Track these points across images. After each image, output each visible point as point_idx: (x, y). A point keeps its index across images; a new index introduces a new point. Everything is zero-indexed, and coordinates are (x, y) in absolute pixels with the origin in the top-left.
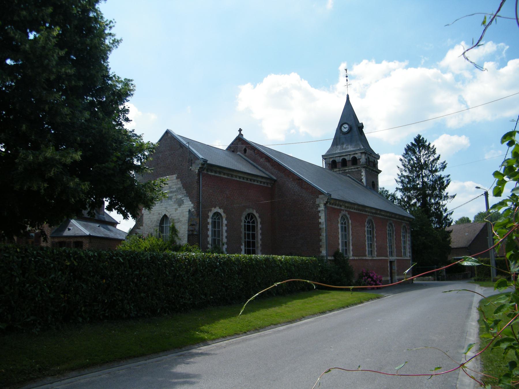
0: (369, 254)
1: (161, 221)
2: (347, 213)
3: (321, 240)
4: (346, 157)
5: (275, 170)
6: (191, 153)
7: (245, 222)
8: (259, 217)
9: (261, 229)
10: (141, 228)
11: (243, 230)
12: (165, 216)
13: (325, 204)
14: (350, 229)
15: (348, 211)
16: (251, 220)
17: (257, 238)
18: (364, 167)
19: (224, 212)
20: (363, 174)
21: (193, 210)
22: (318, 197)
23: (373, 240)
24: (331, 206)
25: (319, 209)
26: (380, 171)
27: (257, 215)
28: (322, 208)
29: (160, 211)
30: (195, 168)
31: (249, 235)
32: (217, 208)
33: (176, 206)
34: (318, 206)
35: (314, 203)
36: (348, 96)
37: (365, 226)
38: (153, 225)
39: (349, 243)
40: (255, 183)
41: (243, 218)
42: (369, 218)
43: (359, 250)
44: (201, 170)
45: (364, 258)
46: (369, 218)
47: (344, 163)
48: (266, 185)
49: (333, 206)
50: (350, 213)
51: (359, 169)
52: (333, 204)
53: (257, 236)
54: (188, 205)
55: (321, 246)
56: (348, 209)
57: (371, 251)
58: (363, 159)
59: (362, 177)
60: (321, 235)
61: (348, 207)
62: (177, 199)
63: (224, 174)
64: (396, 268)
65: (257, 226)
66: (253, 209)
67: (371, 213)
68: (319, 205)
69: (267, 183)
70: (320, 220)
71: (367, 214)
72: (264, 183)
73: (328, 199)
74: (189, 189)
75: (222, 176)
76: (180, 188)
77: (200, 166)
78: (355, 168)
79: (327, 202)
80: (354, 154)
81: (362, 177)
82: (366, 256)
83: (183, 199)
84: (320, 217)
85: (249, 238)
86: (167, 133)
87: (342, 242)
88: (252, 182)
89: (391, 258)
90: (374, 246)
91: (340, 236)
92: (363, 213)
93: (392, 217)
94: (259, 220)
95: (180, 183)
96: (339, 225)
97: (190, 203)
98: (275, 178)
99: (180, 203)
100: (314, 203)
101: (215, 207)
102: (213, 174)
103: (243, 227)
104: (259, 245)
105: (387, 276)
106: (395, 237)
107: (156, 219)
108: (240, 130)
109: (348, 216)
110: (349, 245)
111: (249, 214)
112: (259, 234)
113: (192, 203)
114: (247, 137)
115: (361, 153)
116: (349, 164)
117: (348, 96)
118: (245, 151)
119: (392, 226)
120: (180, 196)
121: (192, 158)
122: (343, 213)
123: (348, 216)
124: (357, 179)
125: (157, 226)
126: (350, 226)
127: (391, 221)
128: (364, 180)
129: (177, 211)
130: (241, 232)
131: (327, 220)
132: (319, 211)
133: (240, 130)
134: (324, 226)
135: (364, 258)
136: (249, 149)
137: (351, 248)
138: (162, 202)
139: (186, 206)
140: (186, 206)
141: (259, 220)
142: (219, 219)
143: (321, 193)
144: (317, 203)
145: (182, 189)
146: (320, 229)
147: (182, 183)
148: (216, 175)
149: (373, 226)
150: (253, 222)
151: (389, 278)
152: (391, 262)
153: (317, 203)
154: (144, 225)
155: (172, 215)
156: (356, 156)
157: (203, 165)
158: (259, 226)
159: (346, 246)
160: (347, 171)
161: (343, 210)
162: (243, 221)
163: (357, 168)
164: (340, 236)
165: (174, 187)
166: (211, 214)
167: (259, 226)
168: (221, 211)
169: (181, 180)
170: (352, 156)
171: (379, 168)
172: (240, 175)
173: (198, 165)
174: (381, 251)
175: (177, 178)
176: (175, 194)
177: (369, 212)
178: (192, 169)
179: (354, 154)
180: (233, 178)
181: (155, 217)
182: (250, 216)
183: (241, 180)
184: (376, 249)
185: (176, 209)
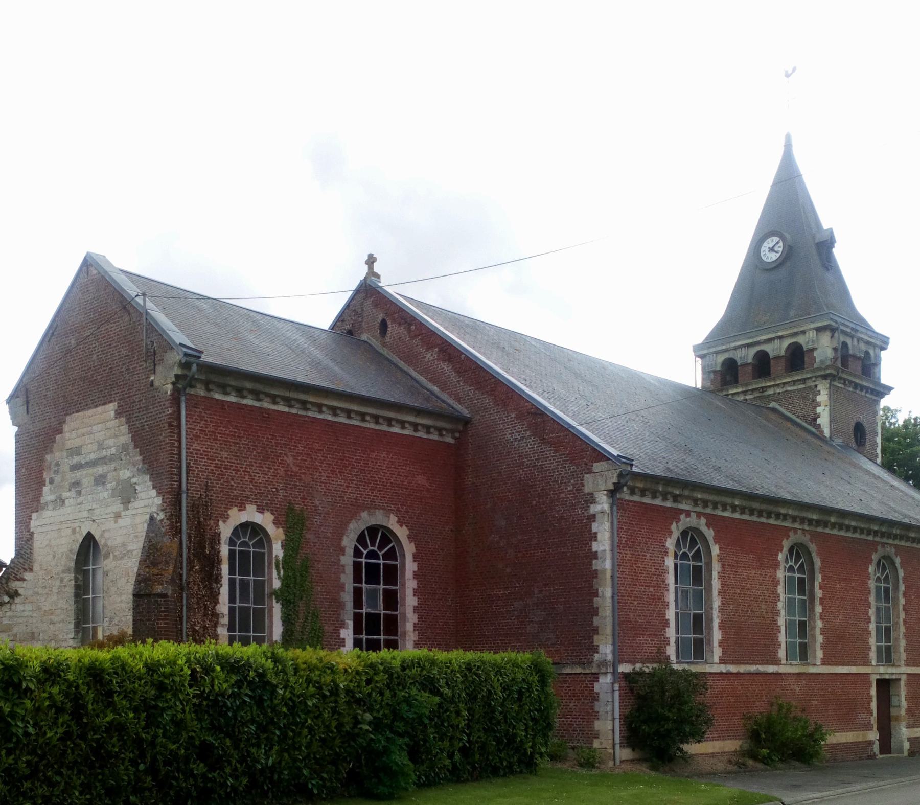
0: (879, 659)
1: (79, 554)
2: (703, 521)
3: (595, 612)
4: (767, 348)
5: (467, 388)
6: (153, 328)
7: (357, 553)
8: (409, 537)
9: (416, 575)
10: (27, 576)
11: (347, 579)
12: (89, 538)
13: (612, 493)
14: (715, 574)
15: (707, 516)
16: (381, 548)
17: (404, 605)
18: (825, 377)
19: (276, 523)
20: (823, 397)
21: (161, 516)
22: (590, 472)
23: (812, 609)
24: (636, 498)
25: (594, 509)
26: (889, 389)
27: (402, 533)
28: (603, 504)
29: (76, 525)
30: (164, 380)
31: (244, 585)
32: (251, 508)
33: (117, 507)
34: (591, 499)
35: (579, 490)
36: (788, 139)
37: (776, 565)
38: (60, 569)
39: (710, 620)
40: (396, 430)
41: (349, 542)
42: (793, 538)
43: (751, 639)
44: (183, 382)
45: (771, 669)
46: (793, 538)
47: (763, 365)
48: (435, 437)
49: (647, 500)
50: (712, 521)
51: (810, 383)
52: (643, 493)
53: (404, 599)
54: (149, 500)
55: (596, 631)
56: (709, 510)
57: (888, 649)
58: (824, 349)
59: (819, 410)
60: (596, 594)
61: (705, 503)
62: (118, 484)
63: (274, 399)
64: (904, 704)
65: (403, 565)
66: (388, 512)
67: (803, 520)
68: (591, 494)
69: (440, 430)
70: (595, 547)
71: (787, 524)
72: (428, 429)
73: (620, 476)
74: (154, 448)
75: (266, 405)
76: (125, 448)
77: (177, 371)
78: (794, 382)
79: (617, 488)
80: (795, 334)
81: (819, 410)
82: (777, 662)
83: (134, 480)
84: (594, 537)
85: (245, 597)
86: (89, 264)
87: (878, 629)
88: (384, 428)
89: (882, 670)
90: (813, 628)
91: (671, 597)
92: (772, 521)
93: (890, 535)
94: (409, 549)
95: (124, 429)
96: (670, 562)
97: (154, 493)
98: (466, 413)
99: (127, 495)
100: (579, 489)
101: (242, 508)
102: (232, 399)
103: (350, 570)
104: (409, 627)
105: (867, 727)
106: (902, 601)
107: (65, 549)
108: (371, 261)
109: (709, 533)
110: (710, 628)
111: (373, 530)
112: (409, 592)
113: (159, 493)
114: (393, 284)
115: (819, 330)
116: (777, 368)
117: (788, 139)
118: (384, 326)
119: (893, 563)
120: (125, 474)
121: (154, 345)
122: (685, 522)
123: (709, 533)
124: (803, 417)
125: (69, 570)
126: (716, 567)
127: (891, 551)
128: (824, 420)
129: (121, 522)
130: (342, 587)
131: (618, 546)
132: (593, 518)
133: (371, 261)
134: (608, 565)
135: (771, 669)
136: (394, 321)
137: (717, 635)
138: (79, 493)
139: (142, 503)
140: (142, 503)
141: (409, 549)
142: (260, 544)
143: (600, 455)
144: (587, 490)
145: (131, 446)
146: (595, 574)
147: (130, 430)
148: (245, 402)
149: (812, 564)
150: (391, 555)
151: (873, 735)
152: (885, 685)
153: (587, 490)
154: (36, 567)
155: (107, 535)
156: (801, 340)
157: (186, 366)
158: (411, 567)
159: (888, 639)
160: (771, 391)
161: (688, 513)
162: (350, 551)
163: (804, 381)
164: (671, 597)
165: (111, 442)
166: (226, 530)
167: (411, 567)
168: (265, 520)
169: (128, 421)
170: (786, 343)
171: (885, 379)
172: (335, 403)
173: (172, 368)
174: (844, 645)
175: (118, 414)
176: (113, 466)
177: (794, 519)
178: (156, 384)
179: (795, 334)
180: (310, 414)
181: (63, 541)
182: (377, 535)
183: (342, 419)
184: (820, 639)
185: (118, 516)
